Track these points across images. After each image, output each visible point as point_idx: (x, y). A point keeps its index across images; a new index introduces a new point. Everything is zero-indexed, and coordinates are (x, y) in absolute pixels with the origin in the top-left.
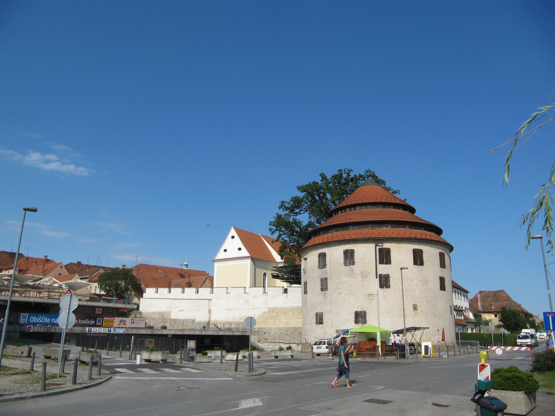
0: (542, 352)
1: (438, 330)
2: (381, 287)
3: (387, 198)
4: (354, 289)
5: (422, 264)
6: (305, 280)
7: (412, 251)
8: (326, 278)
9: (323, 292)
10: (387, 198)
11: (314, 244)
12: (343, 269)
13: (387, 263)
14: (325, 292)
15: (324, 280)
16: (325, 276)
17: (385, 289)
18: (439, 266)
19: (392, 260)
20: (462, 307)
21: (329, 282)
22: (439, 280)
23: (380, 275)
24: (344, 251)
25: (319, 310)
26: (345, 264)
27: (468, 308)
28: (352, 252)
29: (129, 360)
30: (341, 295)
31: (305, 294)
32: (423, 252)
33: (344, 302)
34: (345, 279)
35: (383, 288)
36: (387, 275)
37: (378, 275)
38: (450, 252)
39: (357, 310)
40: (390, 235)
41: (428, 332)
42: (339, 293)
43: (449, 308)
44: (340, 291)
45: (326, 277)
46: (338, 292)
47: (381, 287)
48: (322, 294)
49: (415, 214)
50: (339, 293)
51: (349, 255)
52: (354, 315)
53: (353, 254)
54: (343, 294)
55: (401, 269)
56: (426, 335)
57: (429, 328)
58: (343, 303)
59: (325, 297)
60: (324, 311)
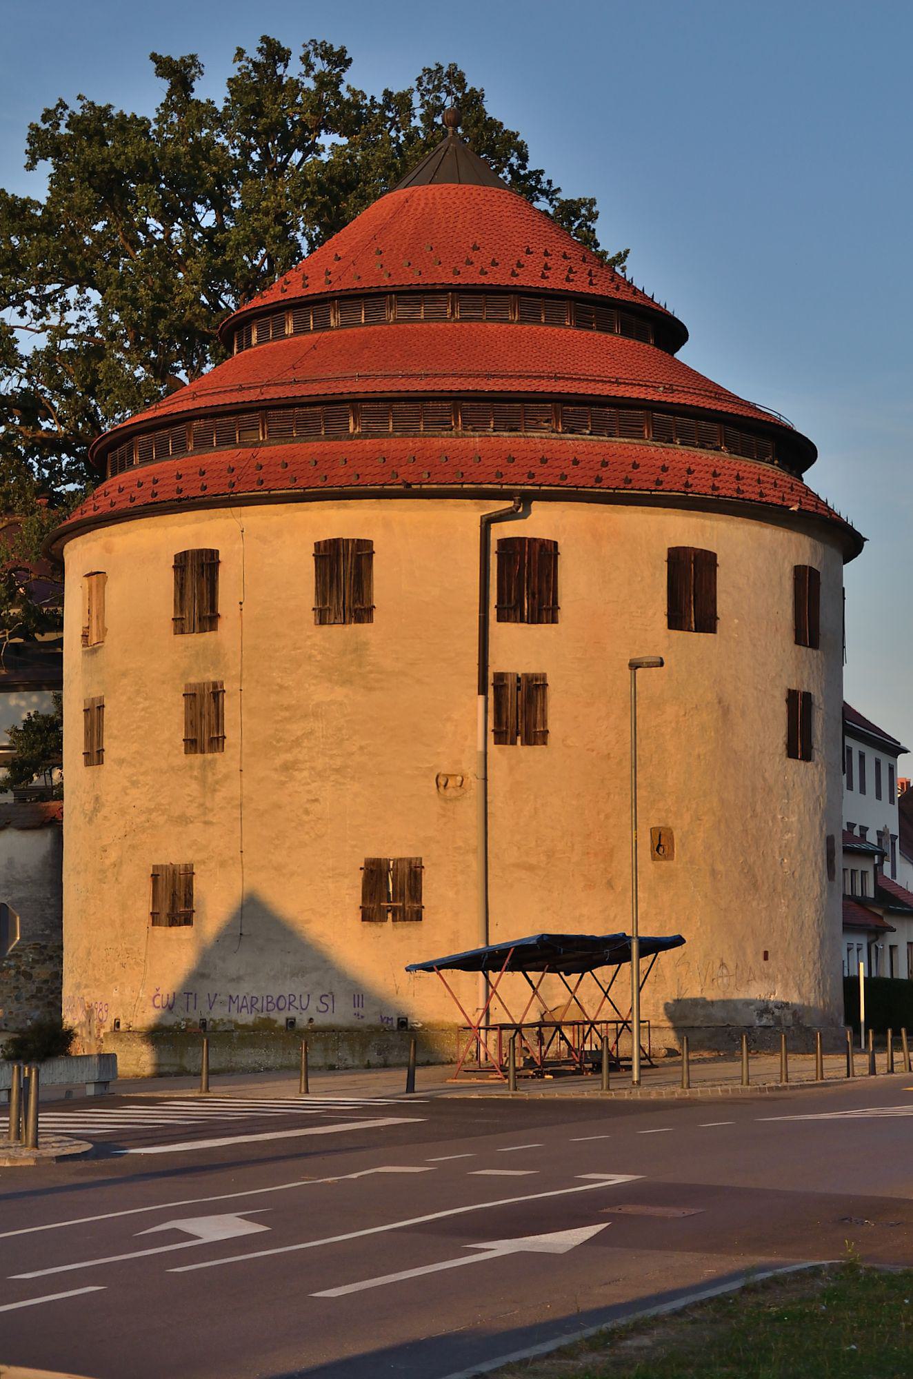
0: (255, 1019)
1: (766, 954)
2: (502, 736)
3: (546, 268)
4: (361, 748)
5: (707, 623)
6: (95, 693)
7: (666, 557)
8: (215, 685)
9: (197, 758)
10: (546, 268)
11: (151, 500)
12: (309, 643)
13: (535, 619)
14: (209, 756)
15: (202, 697)
16: (212, 677)
17: (520, 750)
18: (790, 637)
19: (562, 602)
20: (864, 829)
21: (230, 706)
22: (783, 708)
23: (500, 677)
24: (317, 545)
25: (172, 855)
26: (322, 617)
27: (893, 837)
28: (362, 552)
29: (817, 1079)
30: (296, 773)
31: (87, 764)
32: (716, 565)
33: (307, 812)
34: (320, 694)
35: (514, 743)
36: (536, 677)
37: (491, 680)
38: (846, 561)
39: (374, 854)
40: (558, 471)
41: (718, 964)
42: (287, 767)
43: (821, 846)
44: (289, 757)
45: (213, 679)
46: (278, 762)
47: (502, 736)
48: (191, 768)
49: (682, 355)
50: (287, 767)
51: (346, 567)
52: (358, 879)
53: (364, 565)
54: (306, 773)
55: (634, 666)
56: (708, 980)
57: (678, 941)
58: (305, 818)
59: (208, 788)
60: (199, 857)
